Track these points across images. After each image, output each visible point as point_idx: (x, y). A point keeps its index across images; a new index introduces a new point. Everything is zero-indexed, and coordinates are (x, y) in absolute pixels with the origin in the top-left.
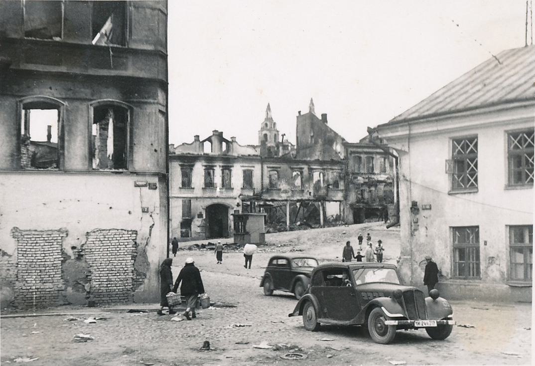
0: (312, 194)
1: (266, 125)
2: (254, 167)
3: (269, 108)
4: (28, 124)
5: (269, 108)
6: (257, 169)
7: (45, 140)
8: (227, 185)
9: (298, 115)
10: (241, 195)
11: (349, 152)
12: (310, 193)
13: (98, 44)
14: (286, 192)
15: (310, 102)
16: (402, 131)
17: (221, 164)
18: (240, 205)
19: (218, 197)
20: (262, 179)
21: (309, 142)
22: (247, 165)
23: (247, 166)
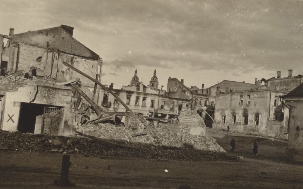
0: (177, 112)
1: (135, 79)
2: (155, 99)
3: (136, 72)
4: (2, 120)
5: (136, 72)
6: (156, 99)
7: (272, 93)
8: (144, 106)
9: (169, 78)
10: (150, 110)
11: (193, 96)
12: (177, 112)
13: (32, 102)
14: (167, 110)
15: (154, 71)
16: (295, 99)
17: (143, 96)
18: (127, 104)
19: (140, 110)
20: (158, 105)
21: (174, 90)
22: (153, 98)
23: (152, 98)
